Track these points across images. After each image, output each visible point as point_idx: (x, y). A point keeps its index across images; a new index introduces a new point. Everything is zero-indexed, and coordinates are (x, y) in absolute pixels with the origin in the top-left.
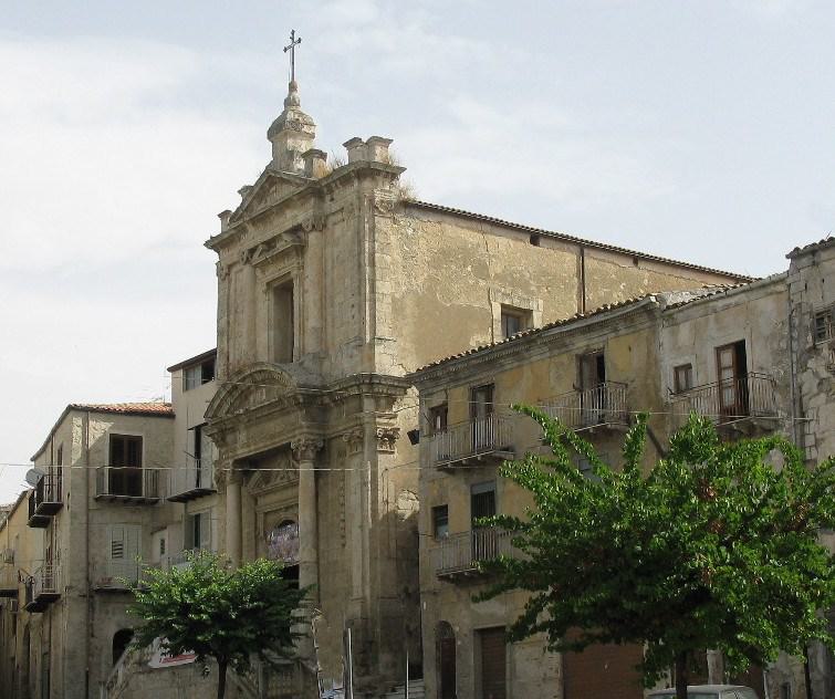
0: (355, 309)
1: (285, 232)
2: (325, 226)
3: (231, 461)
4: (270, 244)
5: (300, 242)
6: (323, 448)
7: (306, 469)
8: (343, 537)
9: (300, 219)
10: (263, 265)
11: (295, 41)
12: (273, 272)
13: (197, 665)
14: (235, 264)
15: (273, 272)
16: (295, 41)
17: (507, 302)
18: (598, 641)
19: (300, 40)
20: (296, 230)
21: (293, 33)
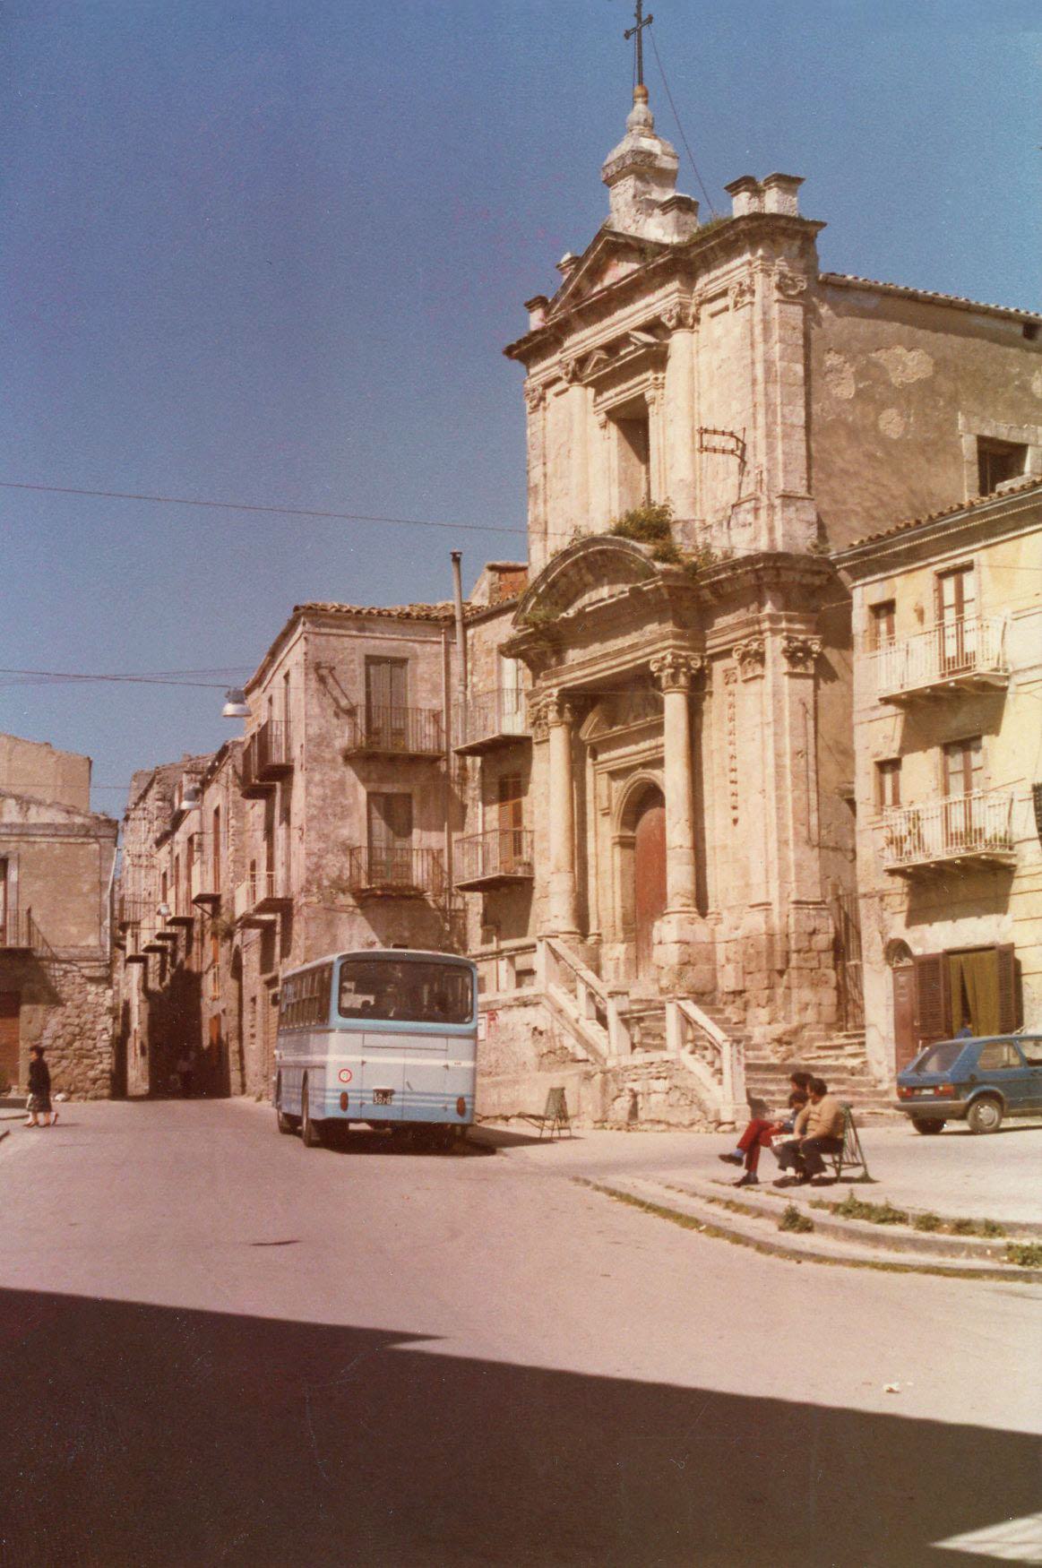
0: (644, 17)
1: (637, 329)
2: (697, 320)
3: (555, 691)
4: (612, 348)
5: (55, 899)
6: (701, 670)
7: (674, 704)
8: (732, 706)
9: (658, 309)
10: (600, 386)
11: (643, 20)
12: (616, 395)
13: (585, 734)
14: (557, 380)
15: (616, 395)
16: (643, 20)
17: (987, 433)
18: (657, 211)
19: (650, 19)
20: (653, 326)
21: (639, 6)
